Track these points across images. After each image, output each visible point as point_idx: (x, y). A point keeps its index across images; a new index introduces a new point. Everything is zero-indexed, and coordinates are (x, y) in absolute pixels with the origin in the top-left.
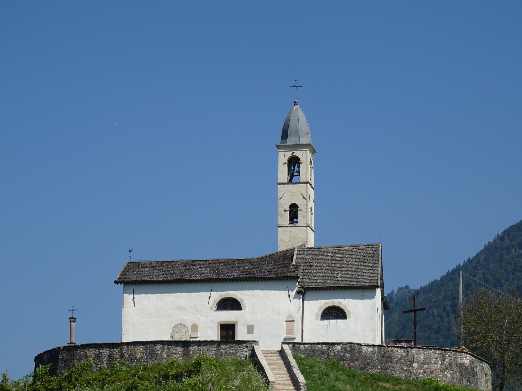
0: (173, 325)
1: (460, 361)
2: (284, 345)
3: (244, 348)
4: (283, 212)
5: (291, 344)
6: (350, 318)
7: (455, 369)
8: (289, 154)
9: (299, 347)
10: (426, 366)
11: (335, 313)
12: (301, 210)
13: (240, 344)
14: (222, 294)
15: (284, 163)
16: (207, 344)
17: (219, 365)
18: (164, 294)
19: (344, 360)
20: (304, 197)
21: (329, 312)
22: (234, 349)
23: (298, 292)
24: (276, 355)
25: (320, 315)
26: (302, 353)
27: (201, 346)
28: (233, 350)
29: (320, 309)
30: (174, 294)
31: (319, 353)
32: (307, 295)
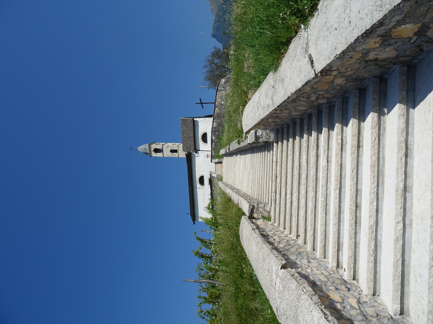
1: (223, 83)
4: (173, 155)
6: (206, 131)
7: (226, 85)
8: (153, 152)
10: (224, 98)
15: (156, 154)
19: (219, 135)
23: (196, 153)
29: (203, 144)
32: (197, 149)
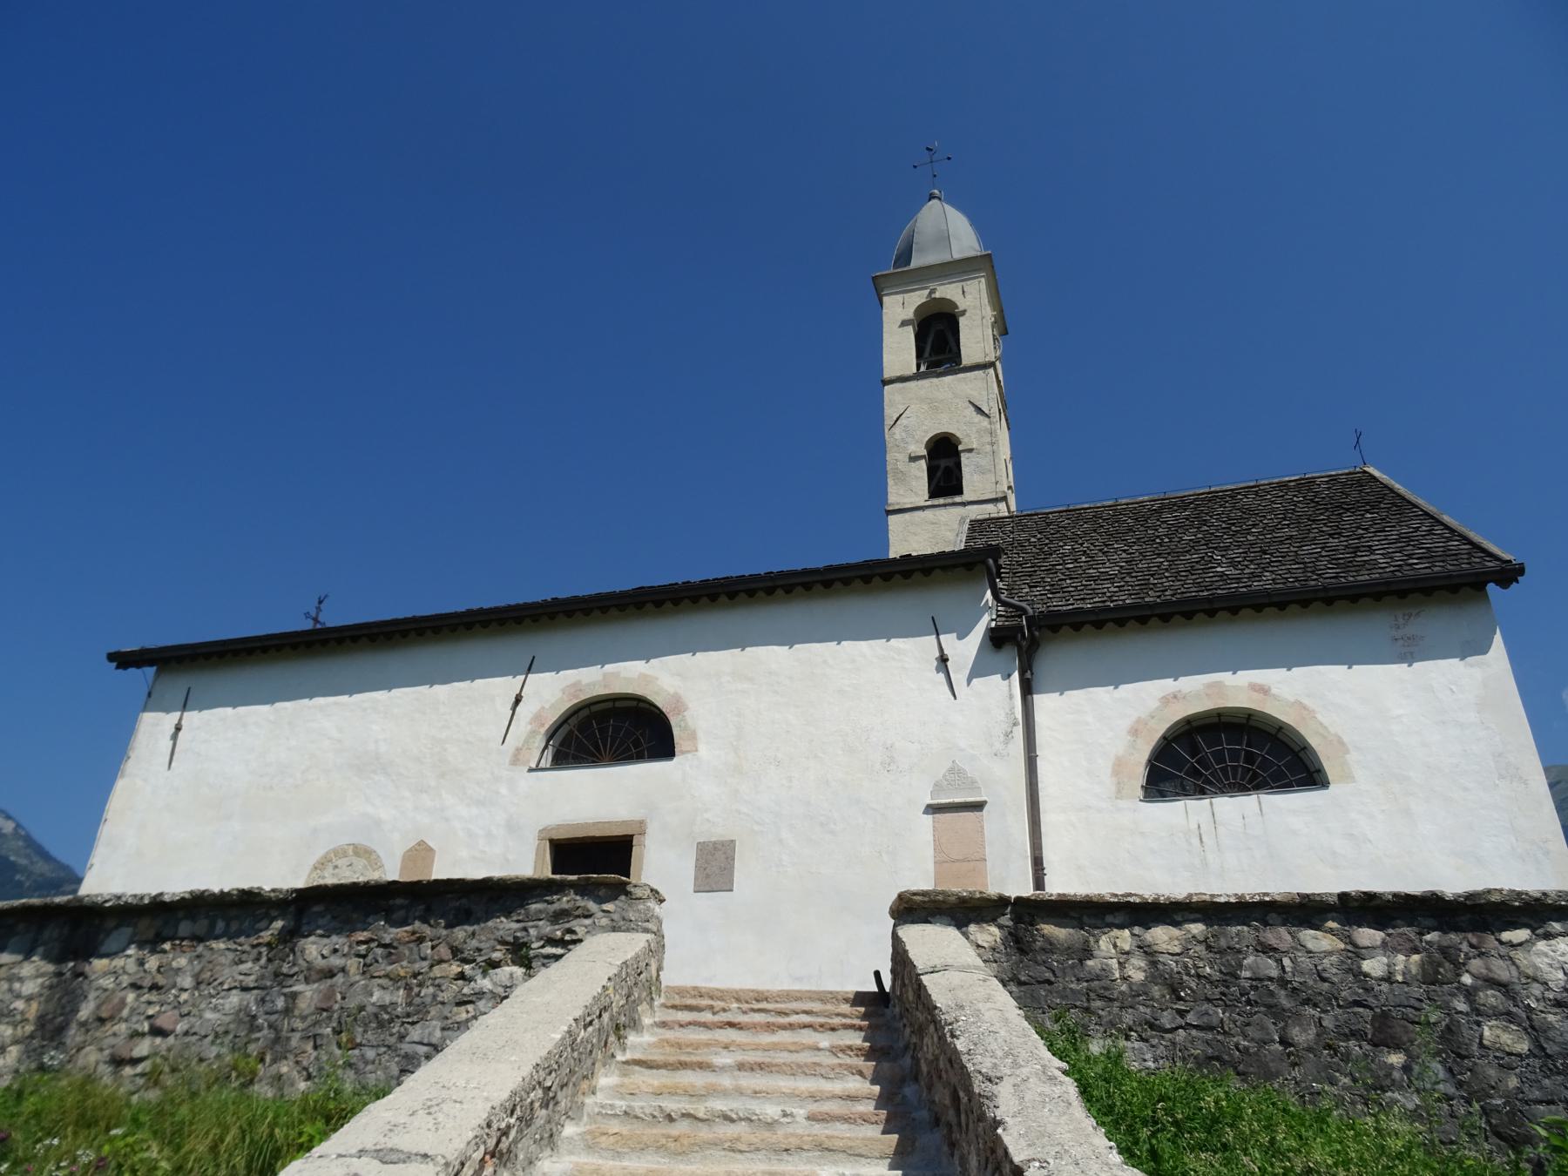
0: (319, 853)
2: (910, 933)
3: (497, 955)
5: (993, 920)
6: (1348, 777)
8: (918, 298)
9: (1087, 952)
11: (1235, 755)
12: (970, 450)
13: (464, 917)
14: (579, 683)
15: (904, 323)
16: (212, 926)
17: (1232, 938)
18: (311, 698)
20: (979, 410)
21: (1194, 751)
22: (401, 969)
23: (997, 639)
24: (825, 1040)
25: (1139, 774)
26: (1128, 1018)
27: (167, 946)
28: (394, 979)
29: (1134, 732)
30: (357, 697)
31: (1328, 1022)
32: (1050, 660)
